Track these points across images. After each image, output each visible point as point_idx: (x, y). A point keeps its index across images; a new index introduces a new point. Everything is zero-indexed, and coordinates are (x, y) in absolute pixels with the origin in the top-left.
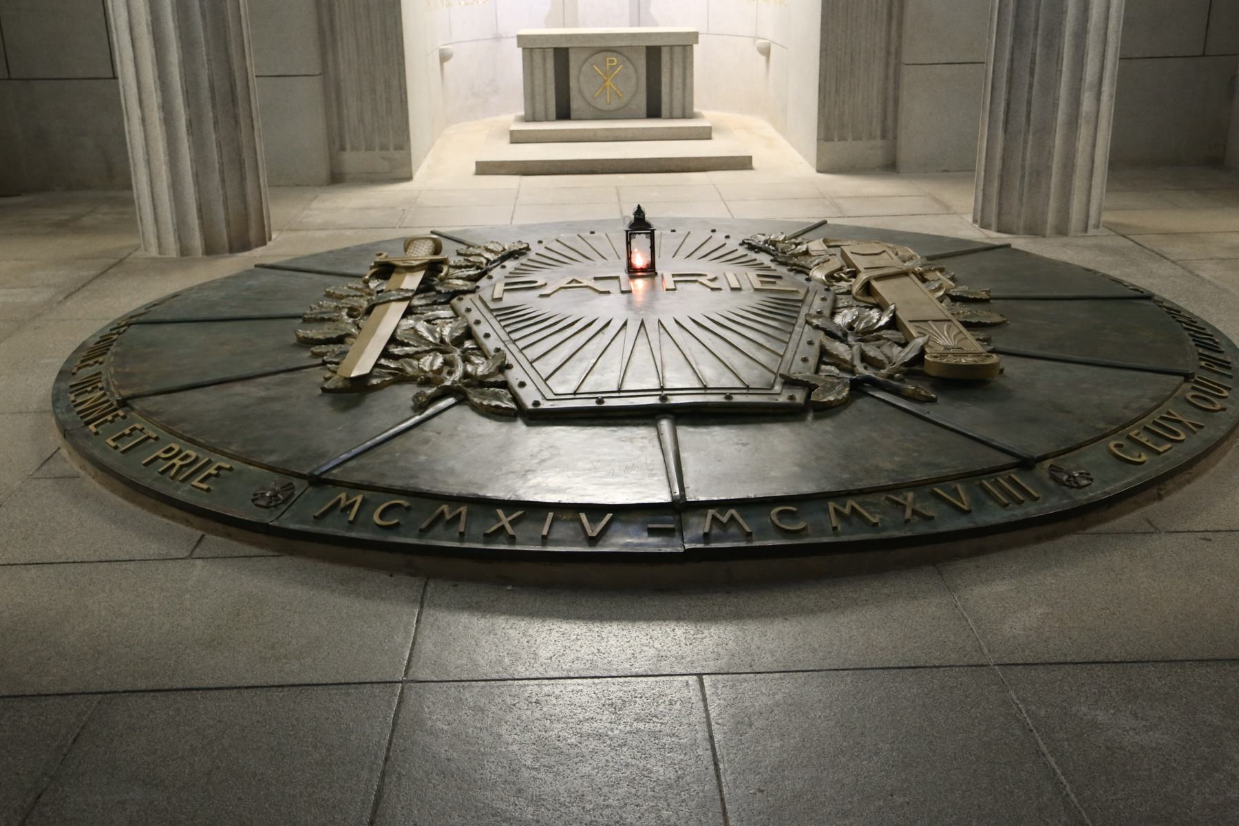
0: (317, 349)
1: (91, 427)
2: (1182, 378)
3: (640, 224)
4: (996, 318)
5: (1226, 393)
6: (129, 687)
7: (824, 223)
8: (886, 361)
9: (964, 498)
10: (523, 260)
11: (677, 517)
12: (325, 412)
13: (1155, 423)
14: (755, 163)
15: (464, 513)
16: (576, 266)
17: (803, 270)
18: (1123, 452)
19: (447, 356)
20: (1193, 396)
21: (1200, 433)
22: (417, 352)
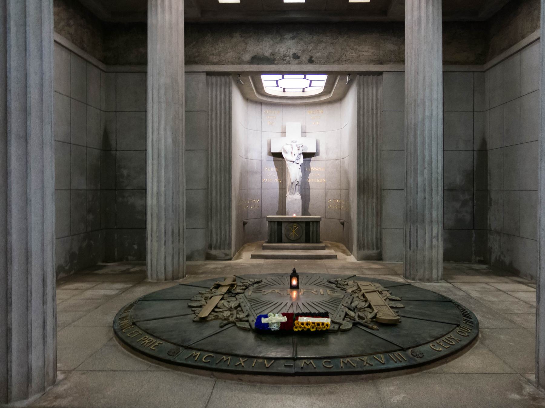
0: (193, 309)
1: (124, 331)
4: (402, 306)
5: (470, 331)
7: (355, 276)
10: (260, 284)
12: (193, 326)
16: (275, 286)
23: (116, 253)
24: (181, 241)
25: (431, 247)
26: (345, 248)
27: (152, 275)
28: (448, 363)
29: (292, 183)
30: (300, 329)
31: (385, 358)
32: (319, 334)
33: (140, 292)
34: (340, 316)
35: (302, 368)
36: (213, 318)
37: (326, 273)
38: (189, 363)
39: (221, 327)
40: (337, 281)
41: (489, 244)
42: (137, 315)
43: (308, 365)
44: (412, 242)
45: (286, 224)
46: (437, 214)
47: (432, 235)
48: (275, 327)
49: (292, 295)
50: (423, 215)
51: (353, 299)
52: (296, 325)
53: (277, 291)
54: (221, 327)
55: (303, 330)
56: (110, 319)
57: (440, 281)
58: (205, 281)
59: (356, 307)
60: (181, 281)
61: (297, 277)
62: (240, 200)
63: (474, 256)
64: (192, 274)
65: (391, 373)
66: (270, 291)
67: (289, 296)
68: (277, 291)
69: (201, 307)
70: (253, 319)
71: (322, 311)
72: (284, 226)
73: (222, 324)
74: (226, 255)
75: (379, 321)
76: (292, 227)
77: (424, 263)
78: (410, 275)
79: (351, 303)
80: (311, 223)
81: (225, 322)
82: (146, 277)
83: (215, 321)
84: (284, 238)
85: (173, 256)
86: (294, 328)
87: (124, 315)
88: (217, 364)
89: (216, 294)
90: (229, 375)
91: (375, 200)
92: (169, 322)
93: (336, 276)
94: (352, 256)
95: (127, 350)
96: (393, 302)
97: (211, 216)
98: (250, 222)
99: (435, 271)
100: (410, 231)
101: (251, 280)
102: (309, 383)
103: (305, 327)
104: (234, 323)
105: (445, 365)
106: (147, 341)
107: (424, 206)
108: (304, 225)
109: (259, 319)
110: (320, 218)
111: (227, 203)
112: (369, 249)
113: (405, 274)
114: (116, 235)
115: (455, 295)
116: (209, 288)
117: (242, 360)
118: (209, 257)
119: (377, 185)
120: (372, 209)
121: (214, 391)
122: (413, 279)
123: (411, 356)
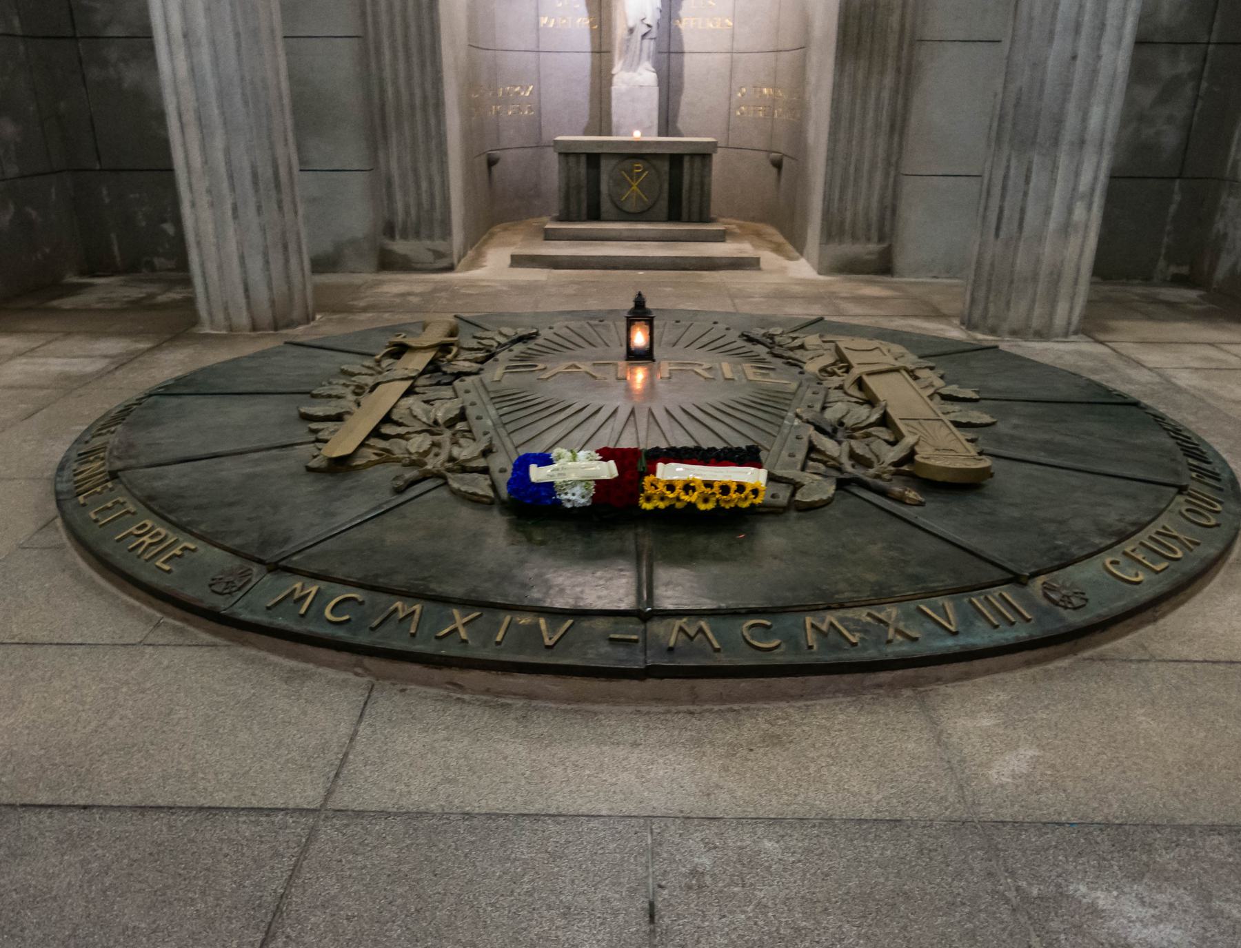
0: (314, 426)
1: (81, 499)
2: (1174, 490)
3: (640, 313)
4: (987, 419)
5: (1219, 508)
6: (27, 800)
7: (821, 319)
8: (874, 459)
9: (951, 616)
10: (531, 344)
11: (642, 627)
12: (307, 488)
13: (1151, 538)
14: (762, 265)
15: (418, 612)
16: (578, 352)
17: (795, 364)
18: (1119, 569)
19: (436, 438)
20: (1188, 510)
21: (1196, 550)
22: (408, 433)
23: (116, 249)
24: (287, 206)
25: (1066, 229)
26: (780, 238)
27: (210, 314)
28: (1161, 622)
29: (631, 31)
30: (662, 505)
31: (957, 608)
32: (727, 521)
33: (173, 363)
34: (792, 455)
35: (671, 649)
36: (374, 458)
37: (731, 310)
38: (280, 622)
39: (399, 491)
40: (772, 337)
41: (1219, 225)
42: (131, 446)
43: (691, 638)
44: (1006, 213)
45: (614, 162)
46: (1102, 115)
47: (1074, 189)
48: (576, 497)
49: (633, 380)
50: (1059, 121)
51: (826, 396)
52: (650, 491)
53: (585, 367)
54: (399, 491)
55: (671, 508)
56: (58, 450)
57: (1073, 338)
58: (366, 334)
59: (841, 424)
60: (299, 333)
61: (650, 322)
62: (471, 83)
63: (1162, 263)
64: (334, 312)
65: (977, 664)
66: (562, 367)
67: (623, 383)
68: (585, 367)
69: (339, 418)
70: (502, 463)
71: (740, 443)
72: (606, 166)
73: (400, 483)
74: (439, 255)
75: (924, 475)
76: (630, 172)
77: (1035, 278)
78: (984, 317)
79: (824, 408)
80: (686, 159)
81: (411, 474)
82: (195, 321)
83: (379, 467)
84: (606, 205)
85: (266, 255)
86: (642, 501)
87: (97, 442)
88: (372, 629)
89: (391, 375)
90: (416, 669)
91: (888, 80)
92: (231, 470)
93: (765, 321)
94: (803, 261)
95: (90, 565)
96: (957, 407)
97: (384, 126)
98: (509, 158)
99: (1062, 308)
100: (1006, 177)
101: (505, 330)
102: (695, 699)
103: (678, 499)
104: (439, 476)
105: (1149, 629)
106: (147, 539)
107: (1066, 86)
108: (665, 167)
109: (522, 464)
110: (714, 145)
111: (428, 86)
112: (855, 238)
113: (970, 314)
114: (105, 192)
115: (1130, 381)
116: (373, 355)
117: (459, 617)
118: (388, 263)
119: (902, 26)
120: (878, 109)
121: (364, 730)
122: (993, 331)
123: (1045, 602)
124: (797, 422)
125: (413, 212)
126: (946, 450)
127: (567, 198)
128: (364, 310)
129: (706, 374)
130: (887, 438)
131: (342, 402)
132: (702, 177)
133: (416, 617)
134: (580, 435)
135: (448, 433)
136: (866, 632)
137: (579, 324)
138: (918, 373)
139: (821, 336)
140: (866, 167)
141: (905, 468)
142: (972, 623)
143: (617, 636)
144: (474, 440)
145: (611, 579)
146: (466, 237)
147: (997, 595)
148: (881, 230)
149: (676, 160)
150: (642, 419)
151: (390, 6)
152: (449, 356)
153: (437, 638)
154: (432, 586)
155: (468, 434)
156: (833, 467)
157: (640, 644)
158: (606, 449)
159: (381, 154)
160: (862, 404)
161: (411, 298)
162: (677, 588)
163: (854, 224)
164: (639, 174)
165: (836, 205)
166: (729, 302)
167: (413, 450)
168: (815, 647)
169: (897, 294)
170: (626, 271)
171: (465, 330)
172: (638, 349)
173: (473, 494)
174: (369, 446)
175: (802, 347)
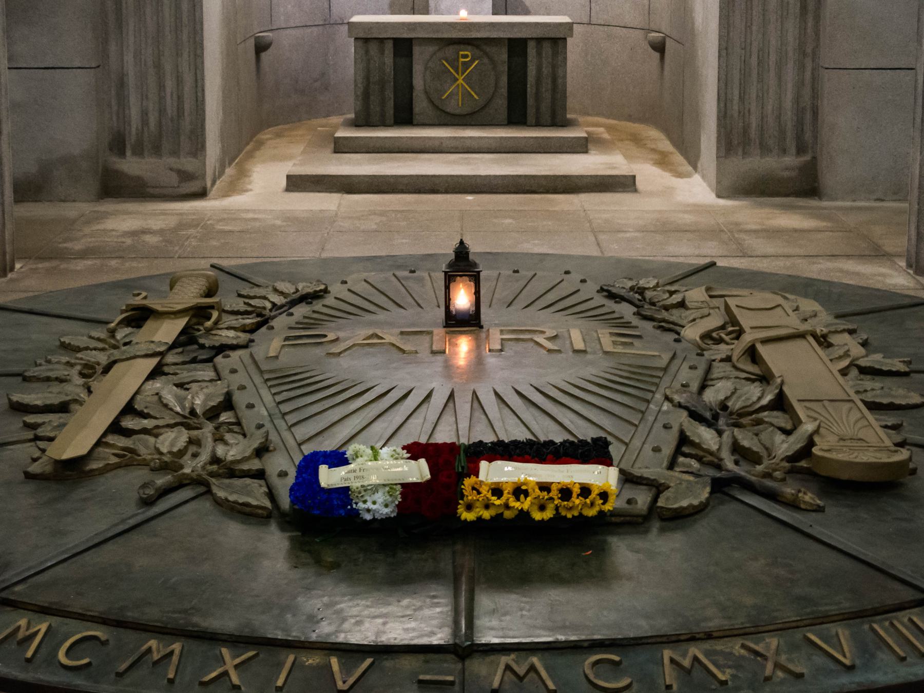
0: (31, 419)
3: (462, 264)
7: (713, 264)
8: (764, 453)
10: (318, 306)
15: (177, 652)
16: (382, 316)
22: (157, 427)
26: (665, 145)
30: (486, 515)
36: (114, 460)
39: (147, 502)
40: (641, 291)
43: (521, 679)
45: (431, 49)
48: (378, 506)
52: (471, 496)
54: (147, 502)
55: (498, 517)
58: (88, 292)
61: (476, 279)
67: (440, 358)
69: (63, 408)
70: (283, 466)
72: (420, 55)
74: (185, 176)
76: (454, 63)
79: (703, 387)
80: (531, 46)
81: (162, 480)
83: (121, 472)
84: (420, 104)
88: (120, 675)
93: (636, 268)
94: (697, 178)
101: (281, 286)
103: (507, 506)
104: (201, 485)
110: (569, 26)
112: (765, 150)
117: (229, 659)
118: (115, 188)
124: (666, 406)
125: (153, 120)
126: (854, 438)
127: (366, 96)
128: (83, 255)
129: (549, 345)
130: (783, 425)
131: (68, 388)
132: (554, 67)
133: (175, 658)
134: (384, 427)
135: (209, 427)
136: (738, 667)
137: (382, 275)
138: (833, 339)
139: (708, 289)
140: (773, 58)
141: (803, 464)
142: (873, 656)
143: (428, 677)
144: (245, 435)
145: (420, 608)
146: (224, 151)
147: (906, 620)
148: (799, 138)
149: (517, 46)
150: (464, 405)
151: (178, 7)
152: (209, 324)
153: (202, 684)
154: (196, 619)
155: (236, 428)
156: (711, 464)
157: (457, 688)
158: (416, 444)
159: (113, 48)
160: (753, 381)
161: (148, 238)
162: (510, 618)
163: (761, 129)
164: (466, 65)
165: (736, 107)
166: (592, 238)
167: (164, 450)
168: (675, 687)
169: (829, 224)
170: (448, 196)
171: (227, 283)
172: (459, 312)
173: (244, 504)
174: (107, 445)
175: (682, 305)
